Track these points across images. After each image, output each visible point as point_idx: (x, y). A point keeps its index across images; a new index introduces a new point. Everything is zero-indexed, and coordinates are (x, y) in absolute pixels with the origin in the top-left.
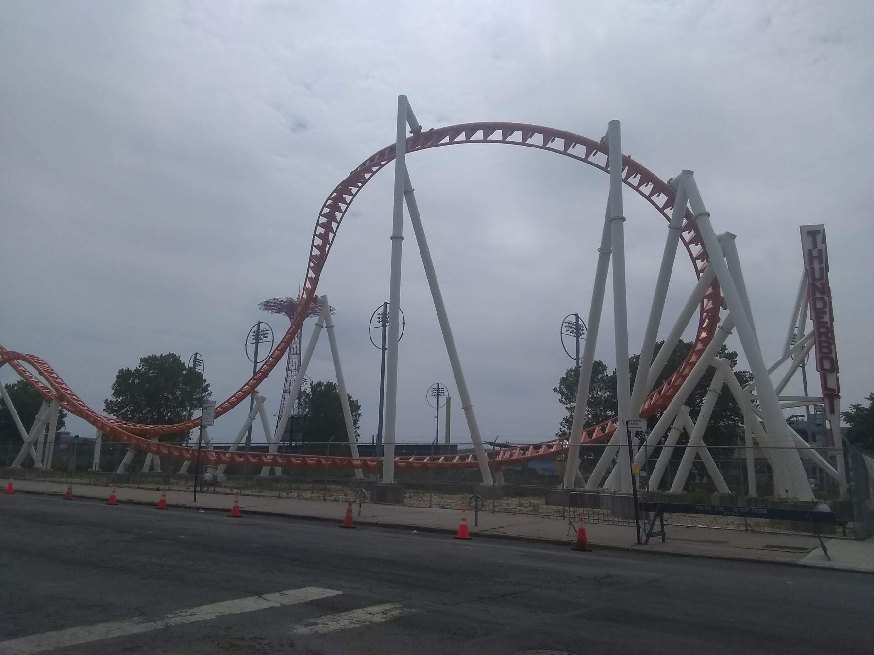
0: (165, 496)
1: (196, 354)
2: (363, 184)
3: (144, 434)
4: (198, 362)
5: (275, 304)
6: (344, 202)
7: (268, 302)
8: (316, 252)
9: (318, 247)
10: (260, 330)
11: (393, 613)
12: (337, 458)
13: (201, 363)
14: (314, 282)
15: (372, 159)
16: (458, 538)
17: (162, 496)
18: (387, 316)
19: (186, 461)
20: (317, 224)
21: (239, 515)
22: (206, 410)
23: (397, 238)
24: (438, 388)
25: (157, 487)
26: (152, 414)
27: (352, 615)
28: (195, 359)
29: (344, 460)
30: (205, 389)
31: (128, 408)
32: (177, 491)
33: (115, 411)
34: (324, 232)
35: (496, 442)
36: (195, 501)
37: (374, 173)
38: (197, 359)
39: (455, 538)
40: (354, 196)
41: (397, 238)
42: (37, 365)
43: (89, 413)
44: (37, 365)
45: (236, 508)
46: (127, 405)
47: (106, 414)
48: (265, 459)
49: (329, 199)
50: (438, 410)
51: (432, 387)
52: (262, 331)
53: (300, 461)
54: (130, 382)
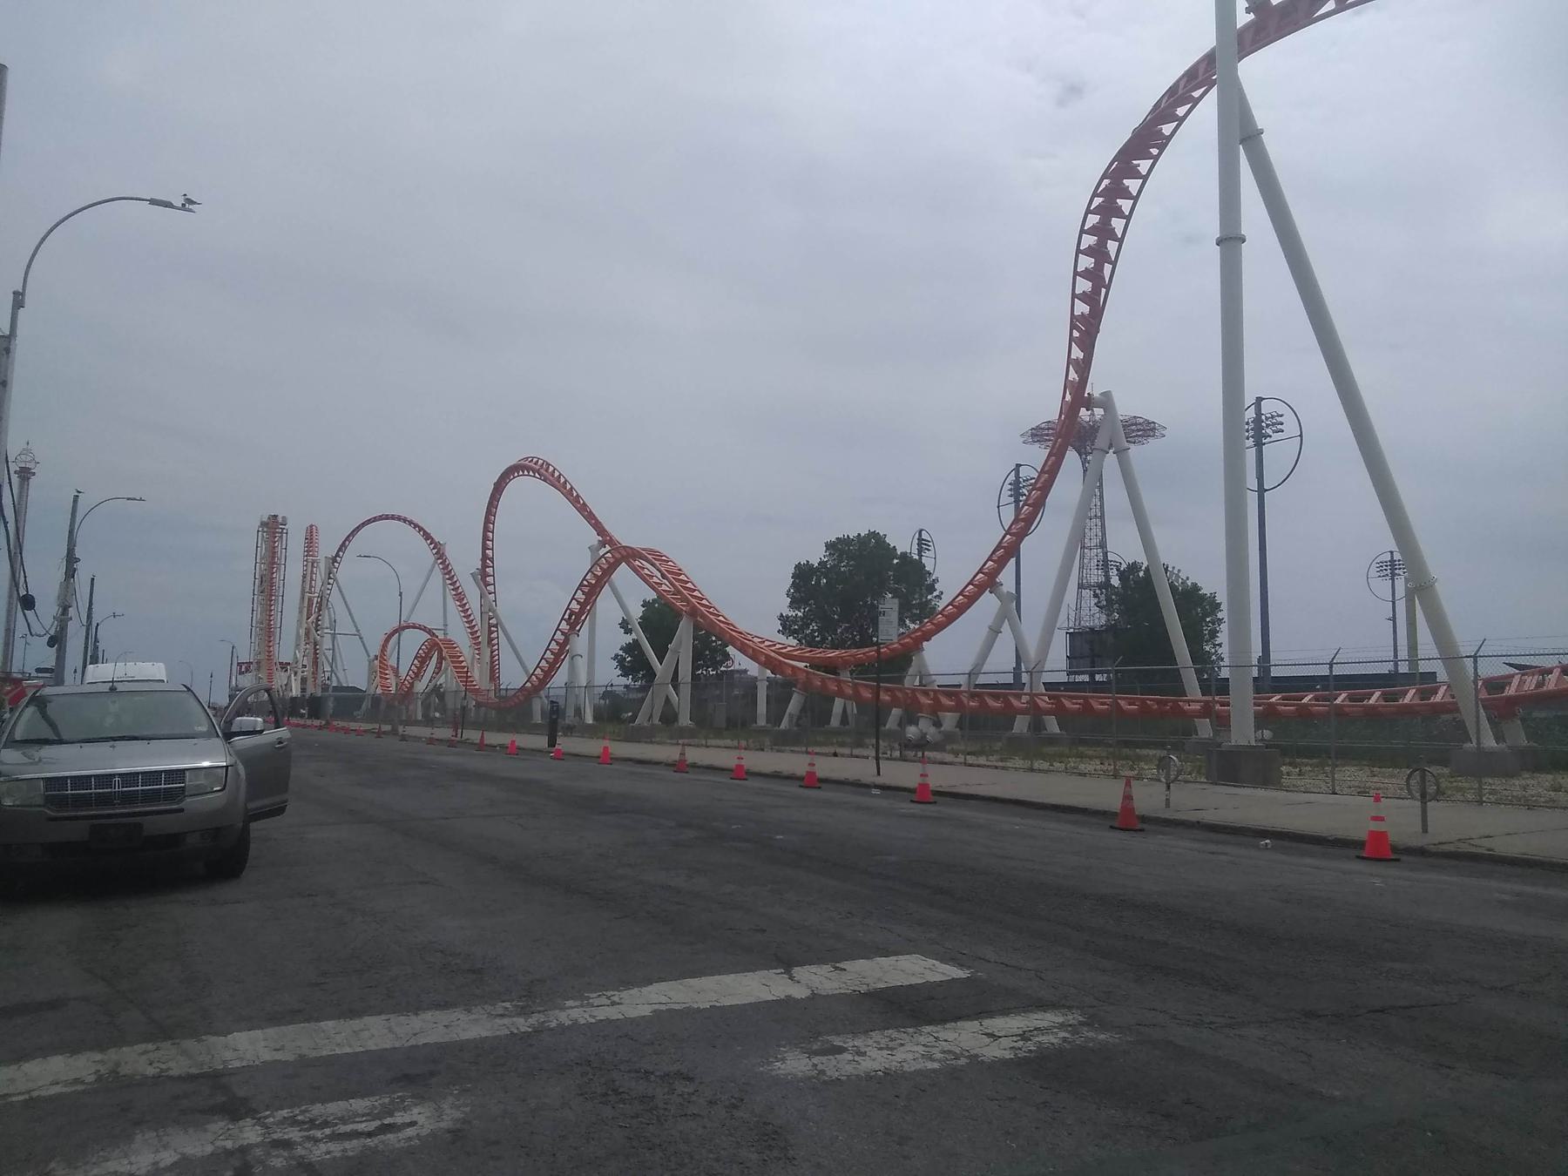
0: (814, 765)
1: (920, 532)
2: (1162, 148)
3: (831, 668)
4: (925, 544)
5: (1051, 431)
6: (1126, 194)
7: (1038, 428)
8: (1082, 308)
9: (1084, 297)
10: (1021, 480)
11: (1044, 1039)
12: (1151, 700)
13: (929, 546)
14: (1083, 367)
15: (1172, 91)
16: (1363, 858)
17: (809, 764)
18: (1263, 424)
19: (894, 709)
20: (1078, 251)
21: (931, 801)
22: (884, 615)
23: (1230, 241)
24: (1392, 561)
25: (833, 751)
26: (852, 634)
27: (942, 1035)
28: (920, 539)
29: (1165, 703)
30: (931, 589)
31: (814, 626)
32: (864, 757)
33: (795, 632)
34: (1092, 265)
35: (1006, 529)
36: (879, 774)
37: (1182, 120)
38: (923, 540)
39: (1358, 857)
40: (1145, 178)
41: (1230, 241)
42: (657, 563)
43: (734, 633)
44: (657, 563)
45: (924, 786)
46: (812, 621)
47: (781, 638)
48: (1015, 702)
49: (1095, 195)
50: (1394, 603)
51: (1378, 560)
52: (1024, 481)
53: (1080, 704)
54: (813, 583)
